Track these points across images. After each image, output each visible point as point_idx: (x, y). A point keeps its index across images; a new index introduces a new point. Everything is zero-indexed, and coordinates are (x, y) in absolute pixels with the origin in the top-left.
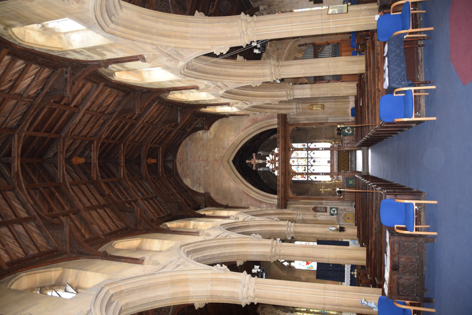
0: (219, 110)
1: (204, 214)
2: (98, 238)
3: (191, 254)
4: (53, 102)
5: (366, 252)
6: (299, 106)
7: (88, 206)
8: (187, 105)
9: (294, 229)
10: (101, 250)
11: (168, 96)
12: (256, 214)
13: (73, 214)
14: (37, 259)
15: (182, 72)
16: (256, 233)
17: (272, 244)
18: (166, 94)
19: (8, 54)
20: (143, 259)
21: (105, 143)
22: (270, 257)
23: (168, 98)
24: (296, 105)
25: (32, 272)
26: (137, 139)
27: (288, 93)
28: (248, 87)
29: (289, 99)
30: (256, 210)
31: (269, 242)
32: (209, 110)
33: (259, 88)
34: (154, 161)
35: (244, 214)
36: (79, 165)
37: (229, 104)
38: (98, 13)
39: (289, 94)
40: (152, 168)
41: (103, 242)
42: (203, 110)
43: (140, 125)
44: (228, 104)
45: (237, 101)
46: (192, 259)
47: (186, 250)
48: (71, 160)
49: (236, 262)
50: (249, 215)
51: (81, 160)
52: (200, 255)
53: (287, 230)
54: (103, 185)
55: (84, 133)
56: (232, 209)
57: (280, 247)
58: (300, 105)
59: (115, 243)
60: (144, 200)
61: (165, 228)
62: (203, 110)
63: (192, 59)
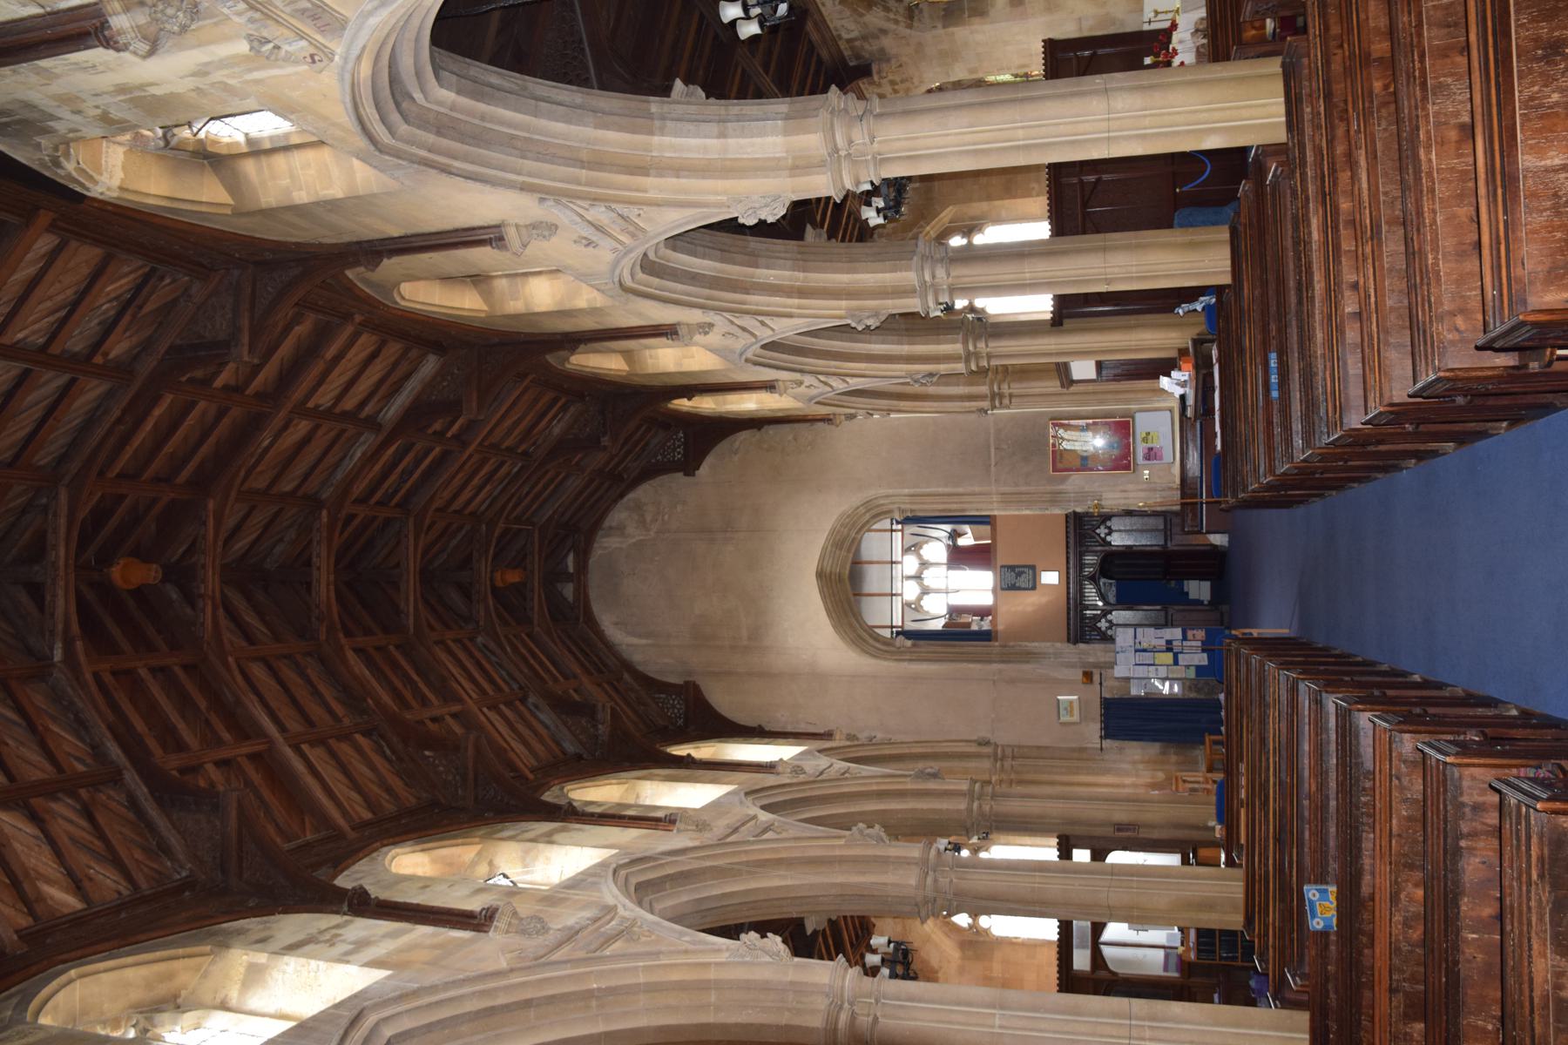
0: (747, 404)
1: (689, 755)
2: (339, 835)
3: (647, 895)
4: (187, 381)
5: (1307, 1036)
6: (934, 277)
7: (36, 775)
8: (497, 340)
9: (992, 807)
10: (344, 881)
11: (568, 359)
12: (861, 757)
13: (364, 735)
14: (123, 915)
15: (628, 282)
16: (869, 819)
17: (969, 790)
18: (563, 353)
19: (52, 228)
20: (672, 818)
21: (353, 516)
22: (916, 905)
23: (568, 366)
24: (965, 343)
25: (601, 783)
26: (457, 505)
27: (840, 141)
28: (842, 329)
29: (849, 185)
30: (795, 780)
31: (914, 850)
32: (706, 405)
33: (877, 331)
34: (514, 577)
35: (818, 754)
36: (139, 593)
37: (676, 333)
38: (370, 112)
39: (933, 285)
40: (511, 603)
41: (342, 860)
42: (683, 404)
43: (470, 456)
44: (769, 386)
45: (797, 376)
46: (652, 913)
47: (634, 881)
48: (105, 570)
49: (802, 919)
50: (834, 760)
51: (148, 574)
52: (683, 897)
53: (969, 810)
54: (350, 655)
55: (457, 505)
56: (780, 740)
57: (951, 869)
58: (941, 273)
59: (398, 855)
60: (304, 747)
61: (563, 802)
62: (683, 404)
63: (658, 243)
